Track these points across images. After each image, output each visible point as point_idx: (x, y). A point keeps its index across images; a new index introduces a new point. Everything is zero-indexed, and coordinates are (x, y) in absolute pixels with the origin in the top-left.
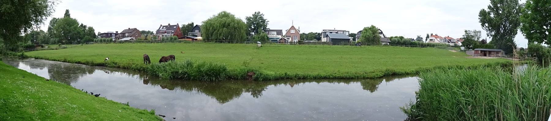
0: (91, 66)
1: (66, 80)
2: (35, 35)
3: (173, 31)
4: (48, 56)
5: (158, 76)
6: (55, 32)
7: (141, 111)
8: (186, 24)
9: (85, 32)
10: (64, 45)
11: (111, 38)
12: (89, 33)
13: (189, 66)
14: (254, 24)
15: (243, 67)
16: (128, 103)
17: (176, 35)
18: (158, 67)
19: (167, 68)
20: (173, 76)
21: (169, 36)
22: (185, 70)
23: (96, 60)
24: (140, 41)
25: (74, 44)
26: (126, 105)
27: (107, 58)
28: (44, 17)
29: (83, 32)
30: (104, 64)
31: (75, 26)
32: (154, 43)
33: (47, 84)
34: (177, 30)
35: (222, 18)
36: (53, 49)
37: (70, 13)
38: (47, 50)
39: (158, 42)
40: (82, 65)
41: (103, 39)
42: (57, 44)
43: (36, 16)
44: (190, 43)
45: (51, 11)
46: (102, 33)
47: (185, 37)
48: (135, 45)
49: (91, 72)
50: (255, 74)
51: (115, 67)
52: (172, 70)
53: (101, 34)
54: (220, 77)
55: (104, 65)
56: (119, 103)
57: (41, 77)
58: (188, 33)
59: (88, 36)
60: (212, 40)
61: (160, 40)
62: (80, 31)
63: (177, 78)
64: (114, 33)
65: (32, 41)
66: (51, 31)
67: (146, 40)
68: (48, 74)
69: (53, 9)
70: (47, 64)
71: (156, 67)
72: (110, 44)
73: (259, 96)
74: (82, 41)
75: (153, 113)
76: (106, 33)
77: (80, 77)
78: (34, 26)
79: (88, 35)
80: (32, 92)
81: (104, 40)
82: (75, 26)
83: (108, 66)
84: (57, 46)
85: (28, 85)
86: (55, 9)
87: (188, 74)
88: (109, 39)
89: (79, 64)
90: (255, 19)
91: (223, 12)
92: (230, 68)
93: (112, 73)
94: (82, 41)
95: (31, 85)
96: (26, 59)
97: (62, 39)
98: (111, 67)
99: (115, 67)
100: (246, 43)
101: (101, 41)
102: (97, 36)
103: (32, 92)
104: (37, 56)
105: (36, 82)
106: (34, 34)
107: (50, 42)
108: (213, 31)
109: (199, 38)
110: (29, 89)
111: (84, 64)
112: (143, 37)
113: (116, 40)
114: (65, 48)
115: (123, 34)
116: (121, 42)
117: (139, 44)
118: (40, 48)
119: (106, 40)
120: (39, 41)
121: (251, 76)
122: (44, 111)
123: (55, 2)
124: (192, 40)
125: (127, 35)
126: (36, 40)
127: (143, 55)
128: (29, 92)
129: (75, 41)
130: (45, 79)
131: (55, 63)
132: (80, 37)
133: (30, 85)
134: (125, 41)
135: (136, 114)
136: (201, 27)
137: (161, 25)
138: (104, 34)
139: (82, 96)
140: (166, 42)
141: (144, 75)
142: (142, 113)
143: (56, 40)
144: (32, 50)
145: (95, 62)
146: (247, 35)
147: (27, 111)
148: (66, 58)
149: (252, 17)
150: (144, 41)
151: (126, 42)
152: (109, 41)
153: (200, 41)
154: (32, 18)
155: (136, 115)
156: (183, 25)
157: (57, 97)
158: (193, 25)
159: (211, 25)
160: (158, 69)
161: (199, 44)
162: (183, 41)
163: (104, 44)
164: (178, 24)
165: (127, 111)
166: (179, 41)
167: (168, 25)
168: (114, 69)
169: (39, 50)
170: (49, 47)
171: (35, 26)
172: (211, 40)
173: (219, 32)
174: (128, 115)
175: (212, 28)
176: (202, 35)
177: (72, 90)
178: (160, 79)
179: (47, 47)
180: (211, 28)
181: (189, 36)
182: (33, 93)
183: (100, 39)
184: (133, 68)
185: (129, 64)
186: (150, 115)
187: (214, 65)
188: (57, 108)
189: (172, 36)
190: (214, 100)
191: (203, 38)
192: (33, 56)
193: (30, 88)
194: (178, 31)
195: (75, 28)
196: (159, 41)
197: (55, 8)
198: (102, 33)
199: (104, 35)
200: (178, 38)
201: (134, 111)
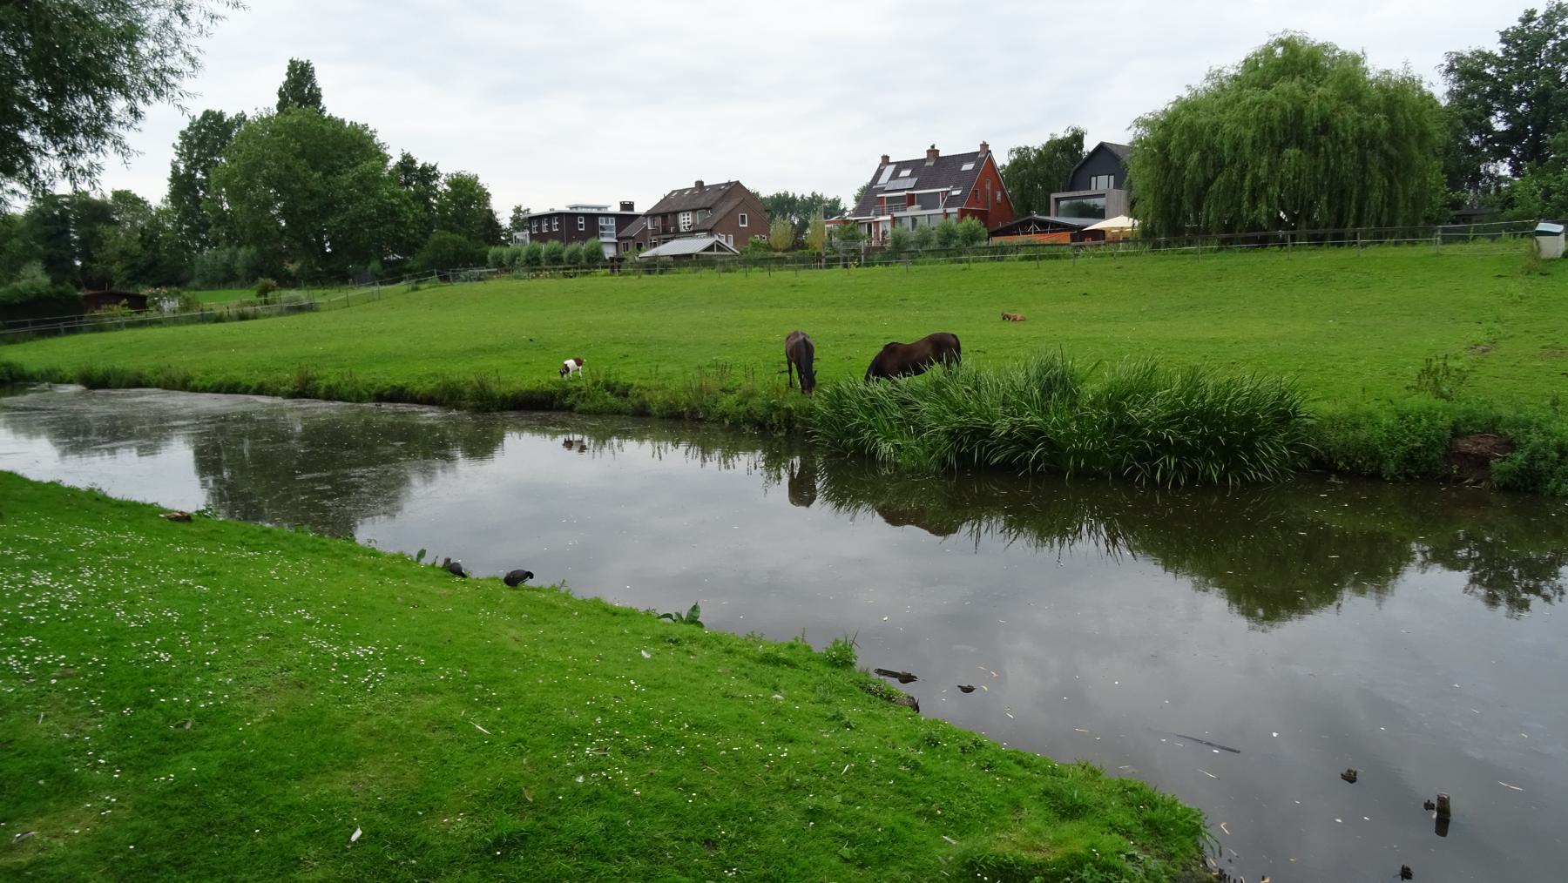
0: (478, 410)
1: (325, 509)
2: (78, 223)
3: (956, 188)
4: (183, 362)
5: (873, 454)
6: (226, 206)
7: (772, 650)
8: (1037, 140)
9: (429, 206)
10: (293, 293)
11: (592, 242)
12: (454, 215)
13: (1055, 395)
14: (1510, 102)
15: (1420, 401)
16: (695, 608)
17: (974, 214)
18: (870, 405)
19: (925, 406)
20: (960, 457)
21: (938, 222)
22: (1032, 418)
23: (503, 377)
24: (766, 259)
26: (686, 622)
27: (571, 363)
28: (118, 105)
29: (418, 209)
31: (366, 166)
32: (846, 266)
33: (177, 544)
34: (981, 184)
35: (1267, 87)
36: (219, 319)
37: (322, 80)
38: (176, 322)
39: (868, 258)
40: (416, 408)
41: (544, 248)
42: (242, 286)
43: (58, 96)
44: (1057, 257)
45: (169, 62)
46: (535, 211)
47: (1028, 223)
48: (737, 278)
49: (482, 446)
50: (1511, 446)
51: (618, 413)
52: (952, 417)
54: (1253, 460)
55: (556, 404)
56: (639, 614)
57: (134, 506)
58: (1048, 198)
59: (449, 235)
60: (1201, 234)
61: (882, 248)
62: (395, 201)
63: (985, 469)
64: (610, 210)
65: (55, 265)
66: (197, 200)
67: (799, 253)
68: (196, 480)
69: (185, 54)
70: (178, 418)
71: (860, 402)
73: (1536, 601)
74: (412, 262)
75: (841, 661)
76: (560, 215)
77: (416, 480)
78: (49, 164)
79: (452, 230)
80: (54, 604)
81: (548, 255)
82: (366, 166)
83: (581, 406)
84: (249, 295)
85: (25, 567)
86: (194, 54)
87: (1049, 444)
88: (583, 247)
89: (402, 407)
90: (1519, 65)
91: (1282, 43)
92: (1326, 408)
93: (606, 449)
95: (54, 561)
96: (12, 394)
97: (282, 255)
98: (597, 413)
99: (618, 413)
100: (1446, 241)
101: (533, 263)
102: (509, 233)
103: (54, 604)
104: (100, 366)
105: (90, 537)
106: (64, 218)
107: (197, 270)
109: (1119, 223)
110: (36, 589)
111: (429, 400)
112: (780, 229)
113: (622, 253)
114: (300, 309)
115: (664, 216)
116: (654, 266)
117: (758, 275)
118: (119, 311)
119: (565, 255)
120: (112, 263)
121: (1482, 462)
122: (151, 712)
123: (189, 7)
124: (1073, 238)
125: (685, 220)
126: (87, 257)
127: (780, 337)
128: (32, 611)
129: (368, 263)
130: (163, 511)
131: (241, 408)
132: (400, 239)
133: (41, 566)
134: (675, 256)
135: (742, 666)
136: (1126, 158)
137: (885, 159)
138: (549, 217)
139: (418, 586)
140: (914, 257)
141: (791, 454)
142: (777, 662)
143: (234, 256)
144: (62, 326)
145: (498, 389)
146: (1454, 184)
147: (24, 738)
148: (312, 372)
149: (1497, 49)
150: (789, 256)
151: (686, 265)
153: (1126, 240)
154: (25, 102)
155: (746, 675)
156: (1019, 151)
157: (241, 612)
158: (1081, 146)
159: (1193, 134)
160: (871, 415)
161: (1115, 264)
162: (1017, 248)
163: (552, 276)
164: (984, 146)
165: (688, 652)
166: (994, 250)
167: (924, 156)
168: (616, 424)
169: (118, 327)
171: (56, 165)
172: (1195, 231)
173: (1247, 183)
174: (695, 675)
175: (1203, 160)
176: (1132, 204)
177: (355, 564)
178: (886, 471)
179: (170, 305)
180: (1195, 156)
181: (1052, 218)
182: (65, 613)
183: (524, 250)
184: (724, 415)
185: (701, 389)
186: (822, 671)
187: (1217, 387)
188: (240, 680)
189: (953, 219)
190: (1215, 603)
191: (1143, 226)
192: (68, 370)
193: (41, 579)
194: (988, 187)
195: (368, 183)
196: (878, 256)
197: (193, 42)
198: (537, 209)
199: (549, 227)
200: (984, 231)
201: (730, 652)
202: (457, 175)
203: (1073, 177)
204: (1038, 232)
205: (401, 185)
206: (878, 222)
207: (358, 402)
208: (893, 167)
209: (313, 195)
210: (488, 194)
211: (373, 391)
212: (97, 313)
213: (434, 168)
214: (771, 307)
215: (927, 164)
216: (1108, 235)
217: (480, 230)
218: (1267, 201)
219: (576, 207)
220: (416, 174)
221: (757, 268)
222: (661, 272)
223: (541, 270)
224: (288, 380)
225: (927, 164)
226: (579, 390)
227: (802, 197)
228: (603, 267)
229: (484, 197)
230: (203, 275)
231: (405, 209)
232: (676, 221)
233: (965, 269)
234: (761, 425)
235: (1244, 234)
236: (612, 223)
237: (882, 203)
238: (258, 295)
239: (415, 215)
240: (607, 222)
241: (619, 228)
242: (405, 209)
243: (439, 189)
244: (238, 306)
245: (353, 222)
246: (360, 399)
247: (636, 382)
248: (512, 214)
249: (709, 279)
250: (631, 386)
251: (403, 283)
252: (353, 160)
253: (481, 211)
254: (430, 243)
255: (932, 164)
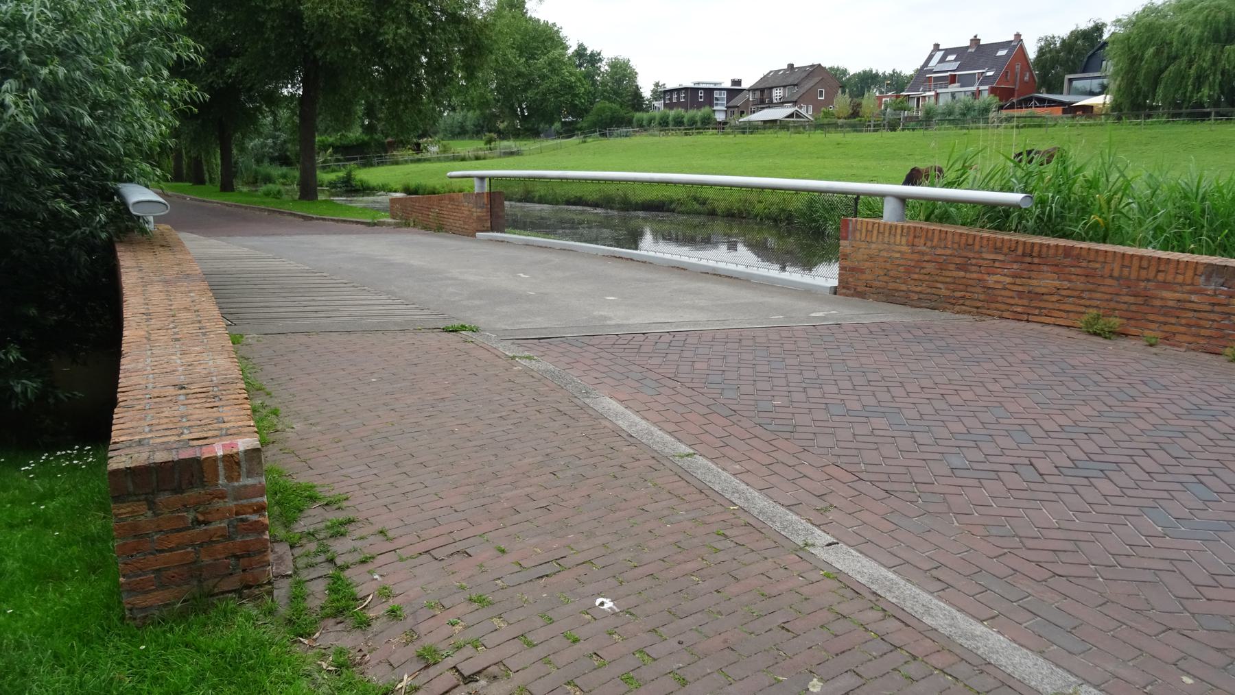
0: (622, 209)
8: (1062, 30)
9: (594, 83)
11: (706, 110)
25: (548, 136)
29: (587, 85)
30: (664, 203)
31: (555, 53)
34: (1011, 67)
38: (439, 160)
41: (672, 113)
42: (471, 138)
46: (669, 87)
47: (1030, 99)
53: (666, 92)
55: (665, 208)
59: (607, 104)
62: (573, 79)
64: (723, 86)
72: (700, 136)
74: (582, 123)
76: (686, 89)
79: (609, 99)
82: (555, 53)
84: (480, 144)
88: (699, 114)
94: (585, 125)
101: (664, 124)
104: (413, 183)
108: (1163, 65)
112: (842, 102)
114: (512, 154)
115: (762, 90)
116: (752, 128)
118: (408, 154)
119: (685, 120)
124: (1065, 112)
125: (777, 94)
137: (937, 47)
138: (678, 90)
152: (699, 124)
164: (1018, 36)
169: (406, 162)
170: (445, 150)
175: (1158, 53)
180: (1151, 50)
184: (756, 216)
185: (746, 201)
195: (555, 66)
198: (670, 85)
199: (678, 98)
202: (615, 59)
203: (1087, 61)
204: (1038, 107)
205: (577, 66)
206: (925, 97)
207: (556, 204)
208: (943, 52)
209: (520, 75)
210: (636, 73)
211: (564, 199)
212: (395, 153)
213: (599, 54)
214: (818, 158)
215: (970, 50)
216: (1095, 109)
217: (629, 101)
218: (1210, 86)
219: (699, 83)
220: (587, 58)
221: (819, 131)
222: (752, 133)
223: (668, 130)
224: (517, 192)
225: (970, 50)
226: (679, 200)
227: (884, 74)
228: (713, 129)
229: (633, 76)
230: (446, 130)
231: (579, 84)
232: (771, 94)
233: (965, 134)
234: (775, 220)
235: (1189, 110)
236: (724, 95)
237: (930, 81)
238: (486, 144)
239: (585, 89)
240: (720, 94)
241: (729, 100)
242: (579, 84)
243: (602, 70)
244: (474, 151)
245: (544, 94)
246: (557, 203)
247: (711, 196)
248: (653, 87)
249: (783, 137)
250: (708, 198)
251: (574, 138)
252: (546, 49)
253: (631, 86)
254: (595, 109)
255: (973, 50)
